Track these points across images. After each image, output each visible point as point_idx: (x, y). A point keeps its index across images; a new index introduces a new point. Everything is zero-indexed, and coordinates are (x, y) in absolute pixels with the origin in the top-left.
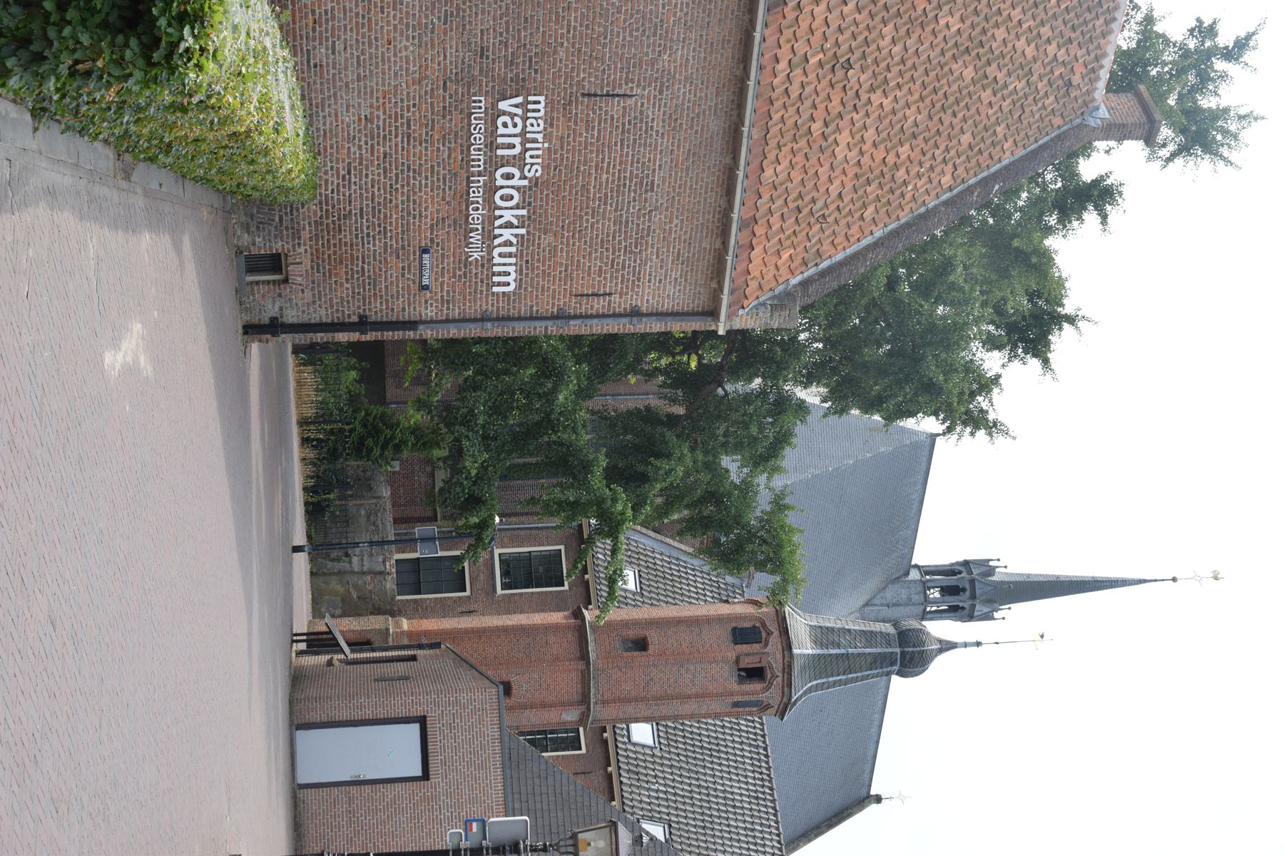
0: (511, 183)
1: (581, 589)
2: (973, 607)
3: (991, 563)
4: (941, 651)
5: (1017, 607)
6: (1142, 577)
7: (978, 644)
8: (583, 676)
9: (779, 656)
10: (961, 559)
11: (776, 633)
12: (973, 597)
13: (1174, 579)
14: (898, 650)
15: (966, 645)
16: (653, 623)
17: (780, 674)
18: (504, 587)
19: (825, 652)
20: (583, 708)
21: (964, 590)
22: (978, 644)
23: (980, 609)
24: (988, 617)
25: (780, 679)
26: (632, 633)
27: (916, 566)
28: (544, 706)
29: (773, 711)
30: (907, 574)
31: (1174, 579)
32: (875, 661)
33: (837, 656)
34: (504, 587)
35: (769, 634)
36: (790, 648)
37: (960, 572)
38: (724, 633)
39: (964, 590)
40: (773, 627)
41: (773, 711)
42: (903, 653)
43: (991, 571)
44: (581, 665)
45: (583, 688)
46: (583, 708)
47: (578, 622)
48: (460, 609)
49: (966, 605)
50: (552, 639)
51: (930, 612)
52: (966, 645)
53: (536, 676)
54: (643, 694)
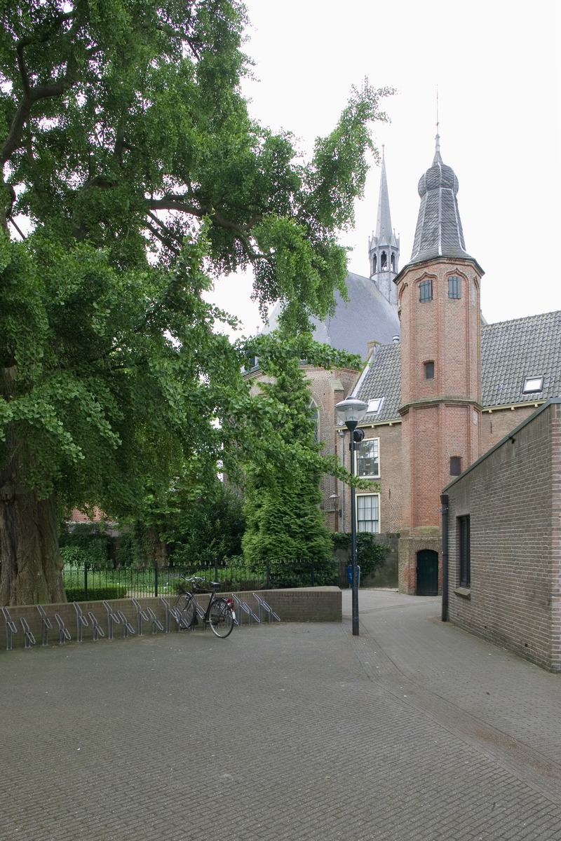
0: (60, 430)
1: (380, 429)
2: (393, 247)
3: (371, 241)
4: (441, 162)
5: (393, 226)
6: (380, 178)
7: (438, 137)
8: (452, 406)
9: (443, 266)
10: (368, 255)
11: (426, 270)
12: (387, 247)
13: (383, 146)
14: (441, 188)
15: (438, 145)
16: (413, 357)
17: (456, 267)
18: (376, 473)
19: (440, 237)
20: (472, 407)
21: (384, 252)
22: (438, 137)
23: (393, 244)
24: (398, 242)
25: (459, 267)
26: (421, 372)
27: (371, 276)
28: (468, 434)
29: (478, 278)
30: (374, 282)
31: (383, 146)
32: (447, 204)
33: (443, 230)
34: (376, 473)
35: (426, 275)
36: (439, 257)
37: (375, 255)
38: (423, 309)
39: (384, 252)
40: (420, 273)
41: (478, 278)
42: (443, 185)
43: (376, 240)
44: (442, 406)
45: (458, 406)
46: (472, 407)
47: (411, 409)
48: (388, 499)
49: (391, 251)
50: (422, 428)
51: (394, 269)
52: (438, 145)
53: (447, 439)
54: (464, 365)
